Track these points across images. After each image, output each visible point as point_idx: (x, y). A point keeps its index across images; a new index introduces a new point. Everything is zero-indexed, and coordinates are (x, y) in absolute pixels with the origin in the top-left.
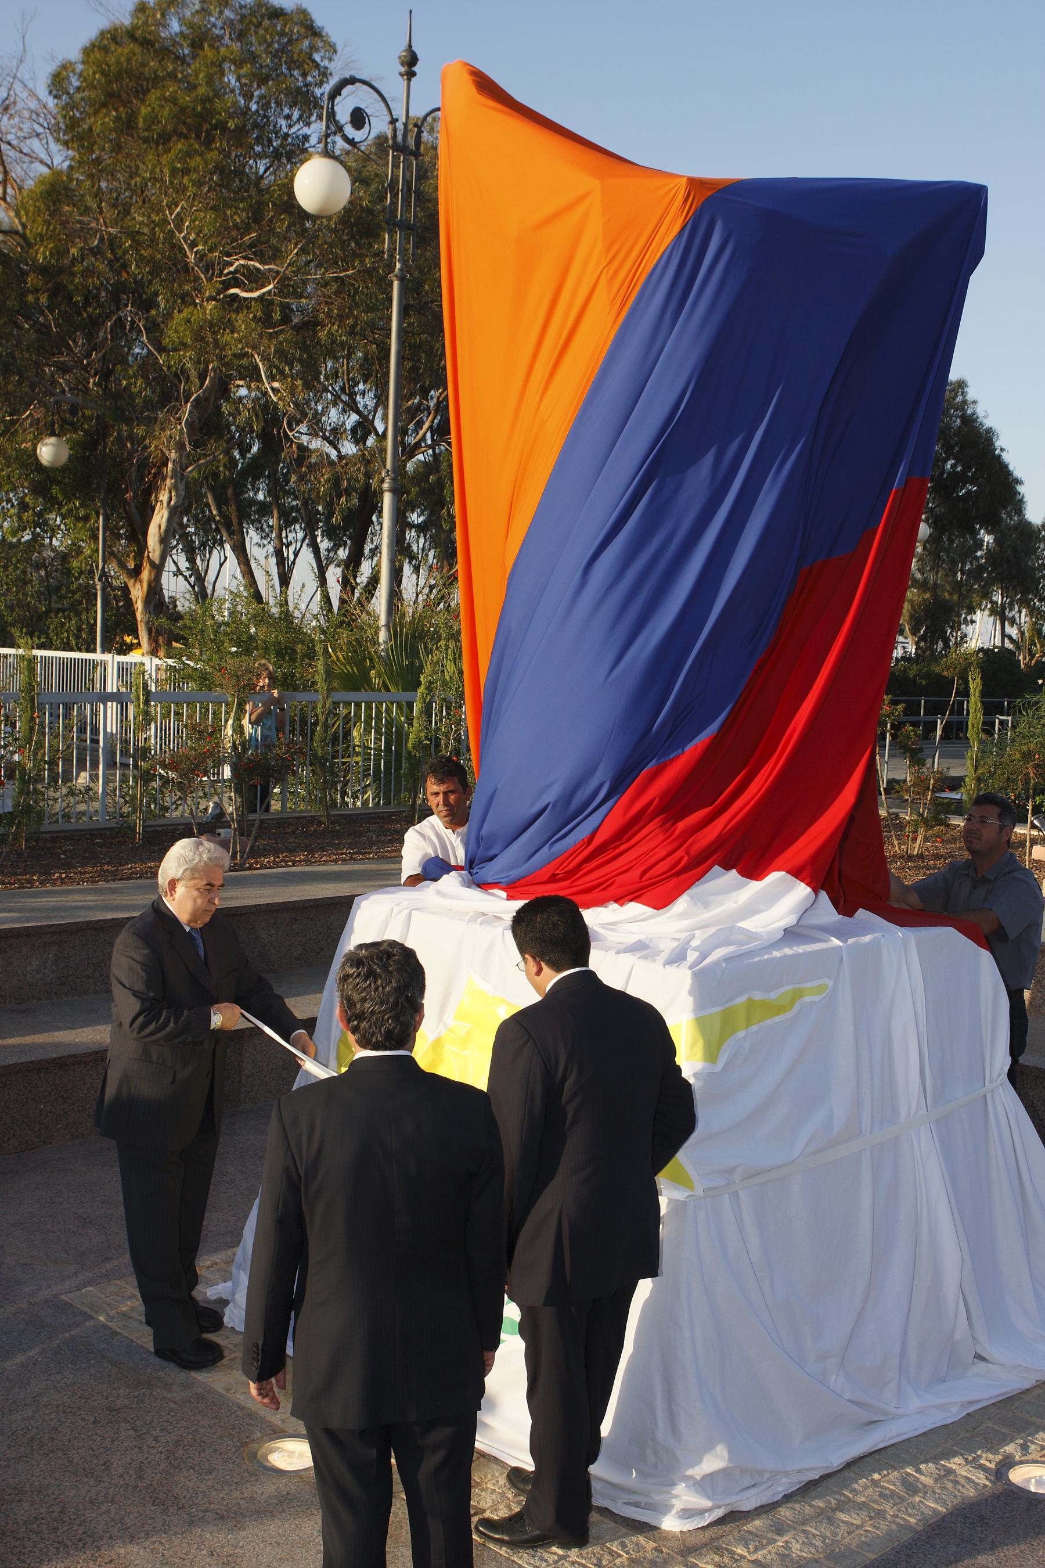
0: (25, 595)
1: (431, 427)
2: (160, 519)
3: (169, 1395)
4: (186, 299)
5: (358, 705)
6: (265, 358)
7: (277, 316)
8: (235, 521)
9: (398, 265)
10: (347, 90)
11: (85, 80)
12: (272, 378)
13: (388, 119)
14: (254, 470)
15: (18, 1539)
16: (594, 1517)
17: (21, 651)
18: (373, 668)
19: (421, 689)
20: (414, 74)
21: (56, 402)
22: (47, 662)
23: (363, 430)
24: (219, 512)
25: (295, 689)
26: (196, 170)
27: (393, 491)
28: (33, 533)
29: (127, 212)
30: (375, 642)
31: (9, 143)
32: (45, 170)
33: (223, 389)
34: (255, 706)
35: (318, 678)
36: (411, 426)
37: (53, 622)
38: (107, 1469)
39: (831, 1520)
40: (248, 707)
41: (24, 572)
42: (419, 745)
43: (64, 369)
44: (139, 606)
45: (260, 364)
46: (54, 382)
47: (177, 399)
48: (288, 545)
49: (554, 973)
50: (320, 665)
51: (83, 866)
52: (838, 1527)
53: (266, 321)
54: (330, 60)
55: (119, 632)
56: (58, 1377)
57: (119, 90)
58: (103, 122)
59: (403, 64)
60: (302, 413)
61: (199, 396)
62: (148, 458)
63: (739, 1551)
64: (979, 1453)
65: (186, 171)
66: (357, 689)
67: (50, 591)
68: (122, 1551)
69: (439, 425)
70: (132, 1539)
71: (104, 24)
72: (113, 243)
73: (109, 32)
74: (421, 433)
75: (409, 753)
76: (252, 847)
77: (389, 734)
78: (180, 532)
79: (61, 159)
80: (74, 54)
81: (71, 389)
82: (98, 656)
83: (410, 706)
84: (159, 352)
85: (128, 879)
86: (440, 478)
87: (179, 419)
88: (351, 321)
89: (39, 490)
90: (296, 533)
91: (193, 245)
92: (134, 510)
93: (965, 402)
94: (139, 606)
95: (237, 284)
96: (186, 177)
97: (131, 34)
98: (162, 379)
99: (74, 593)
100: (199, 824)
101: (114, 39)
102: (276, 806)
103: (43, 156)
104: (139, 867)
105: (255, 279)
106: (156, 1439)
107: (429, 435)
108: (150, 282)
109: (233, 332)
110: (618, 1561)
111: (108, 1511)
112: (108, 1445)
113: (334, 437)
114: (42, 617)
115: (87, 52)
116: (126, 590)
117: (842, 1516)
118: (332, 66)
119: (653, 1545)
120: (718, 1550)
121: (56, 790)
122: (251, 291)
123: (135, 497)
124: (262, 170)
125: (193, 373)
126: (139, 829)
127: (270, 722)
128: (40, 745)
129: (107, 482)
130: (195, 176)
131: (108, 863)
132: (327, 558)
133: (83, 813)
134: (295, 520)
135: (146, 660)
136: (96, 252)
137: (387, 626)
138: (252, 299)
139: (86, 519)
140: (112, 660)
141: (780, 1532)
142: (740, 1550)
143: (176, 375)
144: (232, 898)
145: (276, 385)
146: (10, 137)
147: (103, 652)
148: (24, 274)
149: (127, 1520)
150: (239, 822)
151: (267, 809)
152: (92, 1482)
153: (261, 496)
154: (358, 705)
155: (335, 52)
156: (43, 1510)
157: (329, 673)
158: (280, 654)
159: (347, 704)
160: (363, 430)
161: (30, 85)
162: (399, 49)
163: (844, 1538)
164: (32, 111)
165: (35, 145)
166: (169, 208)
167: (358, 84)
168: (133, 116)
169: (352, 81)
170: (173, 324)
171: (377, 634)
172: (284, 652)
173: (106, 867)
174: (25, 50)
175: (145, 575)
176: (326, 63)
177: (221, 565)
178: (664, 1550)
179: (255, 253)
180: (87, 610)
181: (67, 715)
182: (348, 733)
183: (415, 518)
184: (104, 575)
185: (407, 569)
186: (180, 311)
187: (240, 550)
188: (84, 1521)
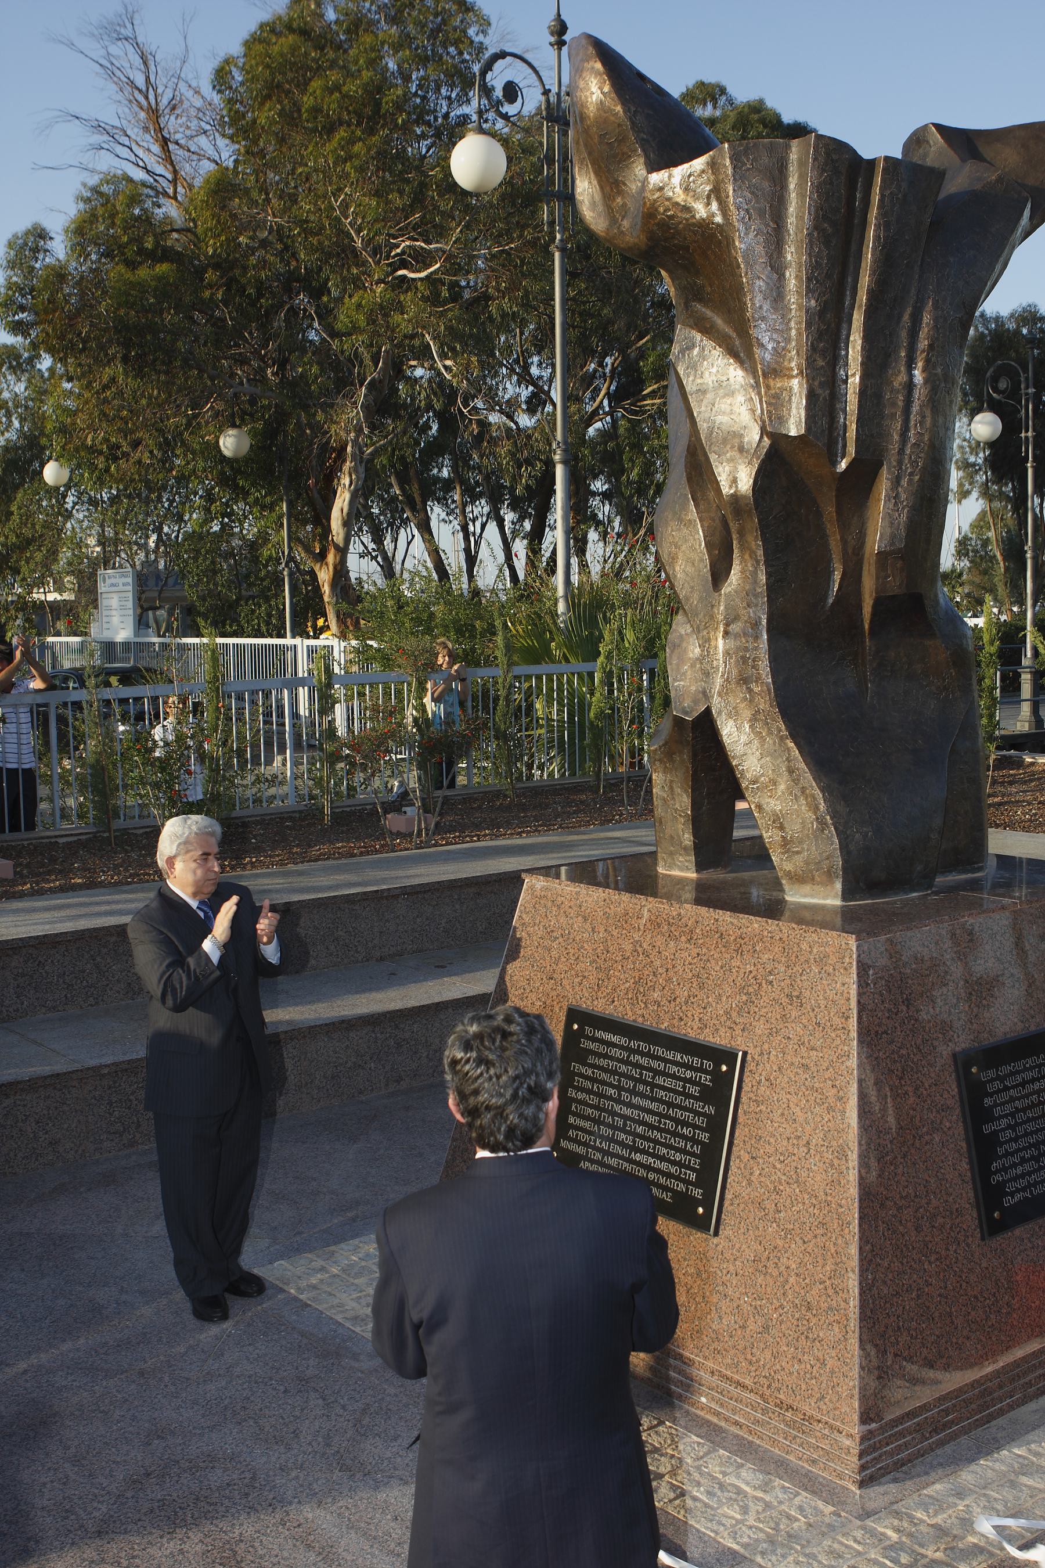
0: (216, 585)
1: (608, 394)
2: (342, 502)
3: (356, 1365)
4: (358, 284)
5: (539, 678)
7: (445, 293)
8: (418, 499)
9: (558, 236)
10: (499, 65)
11: (248, 73)
12: (443, 356)
13: (540, 90)
14: (435, 450)
15: (211, 1504)
17: (205, 640)
18: (553, 640)
19: (601, 659)
21: (235, 395)
22: (239, 649)
23: (537, 402)
24: (403, 490)
25: (477, 664)
26: (357, 156)
27: (564, 462)
28: (222, 523)
29: (294, 199)
30: (554, 615)
31: (177, 143)
32: (212, 166)
33: (397, 369)
34: (435, 684)
35: (498, 653)
36: (588, 394)
37: (243, 610)
38: (297, 1436)
39: (1013, 1484)
40: (429, 686)
41: (213, 562)
42: (601, 715)
43: (242, 361)
44: (326, 589)
46: (233, 375)
47: (352, 384)
48: (474, 521)
50: (499, 639)
51: (273, 849)
52: (1021, 1491)
53: (434, 299)
54: (484, 32)
55: (307, 615)
56: (251, 1349)
57: (282, 80)
58: (267, 115)
60: (477, 388)
61: (373, 379)
62: (328, 442)
63: (919, 1515)
65: (349, 158)
66: (537, 662)
67: (240, 579)
68: (310, 1516)
69: (615, 391)
70: (320, 1503)
71: (265, 16)
72: (280, 232)
73: (267, 24)
74: (598, 400)
75: (591, 723)
76: (437, 824)
77: (571, 705)
78: (364, 514)
79: (227, 155)
80: (236, 49)
81: (248, 380)
82: (288, 641)
83: (591, 675)
84: (332, 338)
85: (316, 860)
86: (618, 444)
87: (355, 403)
89: (224, 481)
90: (482, 507)
91: (358, 232)
92: (316, 495)
94: (326, 589)
95: (404, 265)
97: (290, 28)
98: (336, 366)
99: (262, 580)
100: (383, 803)
101: (273, 31)
102: (461, 780)
103: (211, 152)
104: (325, 848)
105: (422, 259)
106: (344, 1407)
107: (606, 402)
108: (320, 269)
109: (402, 314)
110: (796, 1525)
111: (297, 1477)
112: (298, 1414)
113: (509, 410)
114: (233, 605)
115: (248, 44)
116: (313, 574)
117: (1024, 1480)
118: (487, 41)
119: (831, 1509)
120: (897, 1514)
121: (243, 778)
122: (419, 271)
123: (317, 483)
124: (424, 151)
125: (367, 357)
126: (327, 810)
127: (454, 699)
128: (228, 732)
129: (289, 470)
130: (357, 163)
131: (297, 846)
132: (513, 532)
133: (274, 797)
134: (480, 495)
135: (334, 642)
136: (264, 244)
137: (566, 597)
138: (421, 279)
139: (271, 508)
140: (302, 644)
141: (960, 1495)
142: (920, 1515)
143: (350, 360)
144: (408, 877)
145: (448, 363)
146: (178, 136)
147: (294, 637)
148: (200, 272)
149: (315, 1486)
150: (423, 799)
151: (452, 784)
152: (282, 1449)
153: (445, 473)
154: (539, 678)
155: (489, 24)
156: (235, 1476)
157: (509, 648)
158: (459, 632)
159: (528, 678)
160: (537, 402)
161: (194, 84)
162: (548, 18)
163: (1025, 1501)
164: (199, 109)
165: (203, 141)
166: (334, 195)
167: (508, 58)
168: (297, 107)
169: (503, 55)
170: (344, 309)
171: (556, 604)
172: (462, 630)
173: (295, 850)
174: (187, 50)
175: (331, 558)
176: (480, 38)
177: (409, 544)
178: (843, 1514)
179: (419, 234)
180: (276, 596)
181: (253, 702)
182: (530, 707)
183: (599, 485)
184: (291, 559)
185: (593, 535)
186: (350, 296)
187: (425, 528)
188: (274, 1487)
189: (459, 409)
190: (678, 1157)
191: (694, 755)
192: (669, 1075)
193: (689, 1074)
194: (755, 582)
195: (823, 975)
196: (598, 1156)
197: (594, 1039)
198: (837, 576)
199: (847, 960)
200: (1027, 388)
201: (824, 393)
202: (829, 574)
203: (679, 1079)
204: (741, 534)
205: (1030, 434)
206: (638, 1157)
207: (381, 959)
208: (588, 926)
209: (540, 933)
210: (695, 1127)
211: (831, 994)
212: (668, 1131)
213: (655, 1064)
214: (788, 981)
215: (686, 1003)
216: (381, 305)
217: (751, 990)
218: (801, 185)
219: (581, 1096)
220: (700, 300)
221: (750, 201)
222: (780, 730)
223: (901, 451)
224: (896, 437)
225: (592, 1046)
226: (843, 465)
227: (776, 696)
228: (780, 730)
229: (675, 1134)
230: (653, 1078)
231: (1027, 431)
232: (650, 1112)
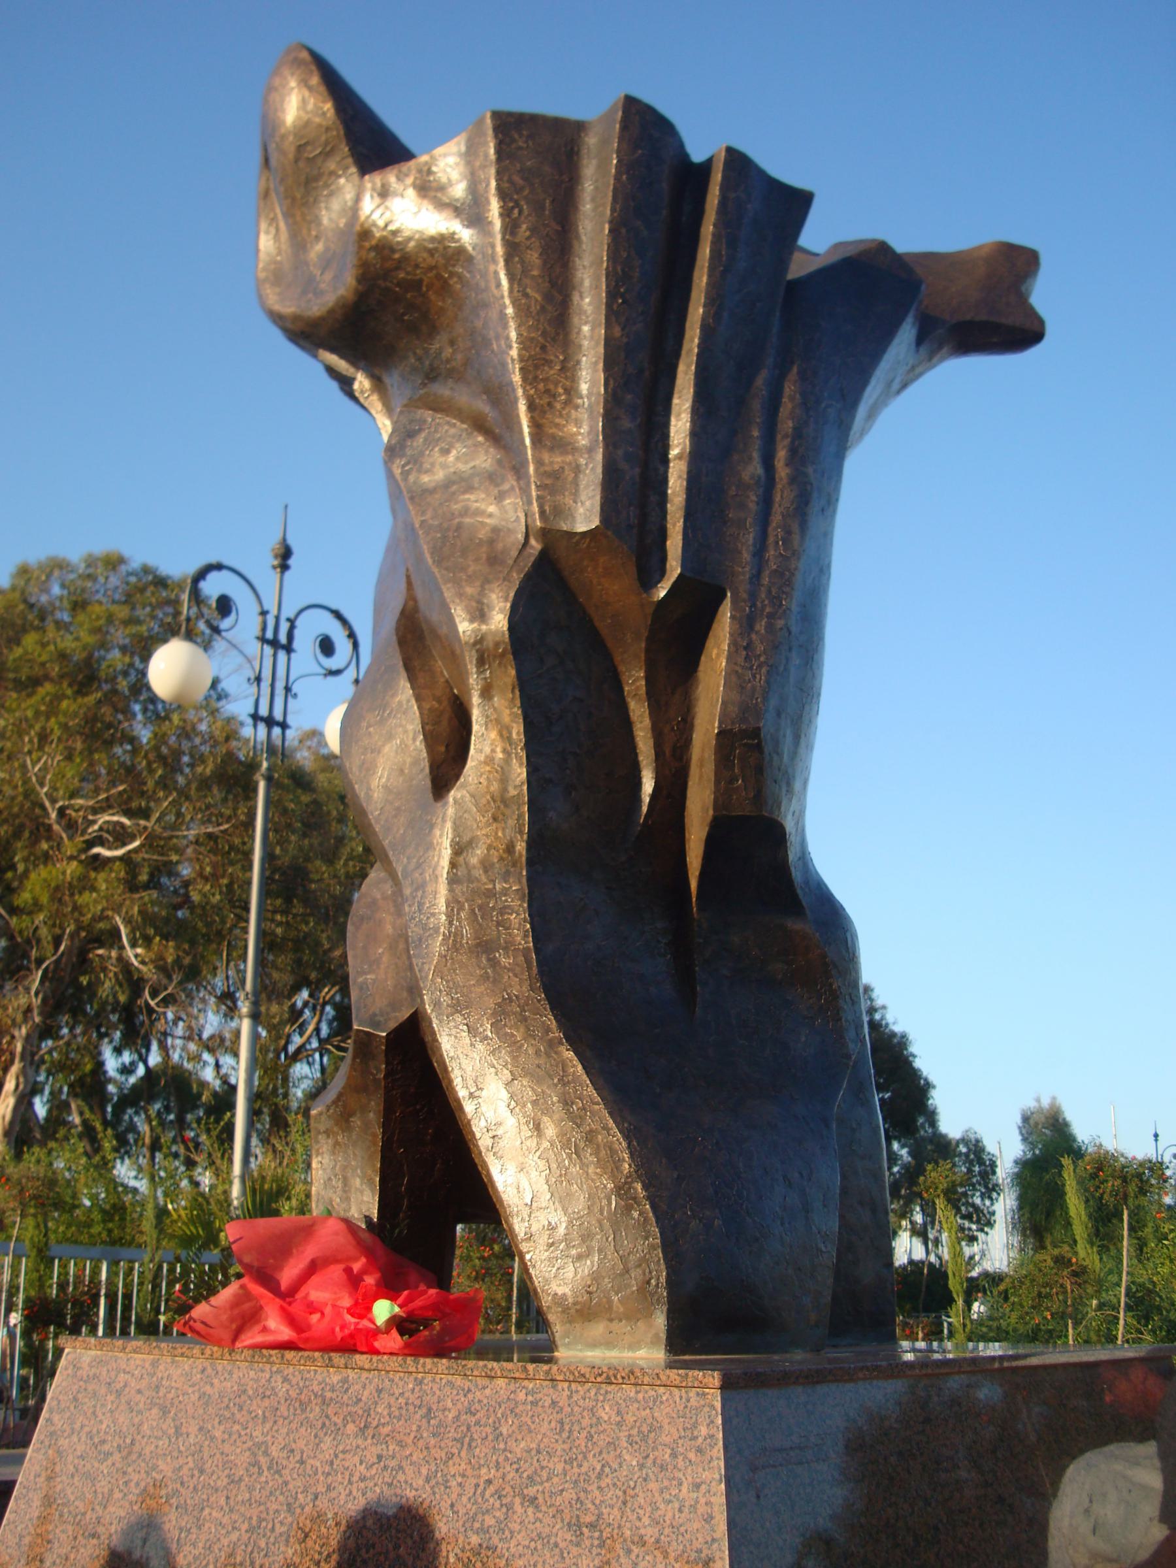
4: (46, 858)
6: (128, 921)
10: (213, 576)
12: (134, 945)
13: (258, 610)
45: (122, 928)
59: (276, 557)
64: (1037, 1152)
69: (324, 987)
88: (225, 881)
95: (99, 841)
96: (53, 720)
105: (120, 836)
122: (116, 848)
162: (272, 541)
167: (225, 573)
169: (219, 567)
189: (146, 1001)
194: (504, 780)
195: (650, 1471)
198: (648, 786)
199: (703, 1430)
201: (632, 473)
202: (638, 784)
204: (486, 693)
208: (168, 1425)
209: (80, 1448)
211: (668, 1512)
214: (570, 1495)
216: (70, 883)
217: (490, 1521)
221: (522, 189)
222: (548, 1030)
223: (757, 576)
224: (746, 556)
227: (541, 972)
228: (548, 1030)
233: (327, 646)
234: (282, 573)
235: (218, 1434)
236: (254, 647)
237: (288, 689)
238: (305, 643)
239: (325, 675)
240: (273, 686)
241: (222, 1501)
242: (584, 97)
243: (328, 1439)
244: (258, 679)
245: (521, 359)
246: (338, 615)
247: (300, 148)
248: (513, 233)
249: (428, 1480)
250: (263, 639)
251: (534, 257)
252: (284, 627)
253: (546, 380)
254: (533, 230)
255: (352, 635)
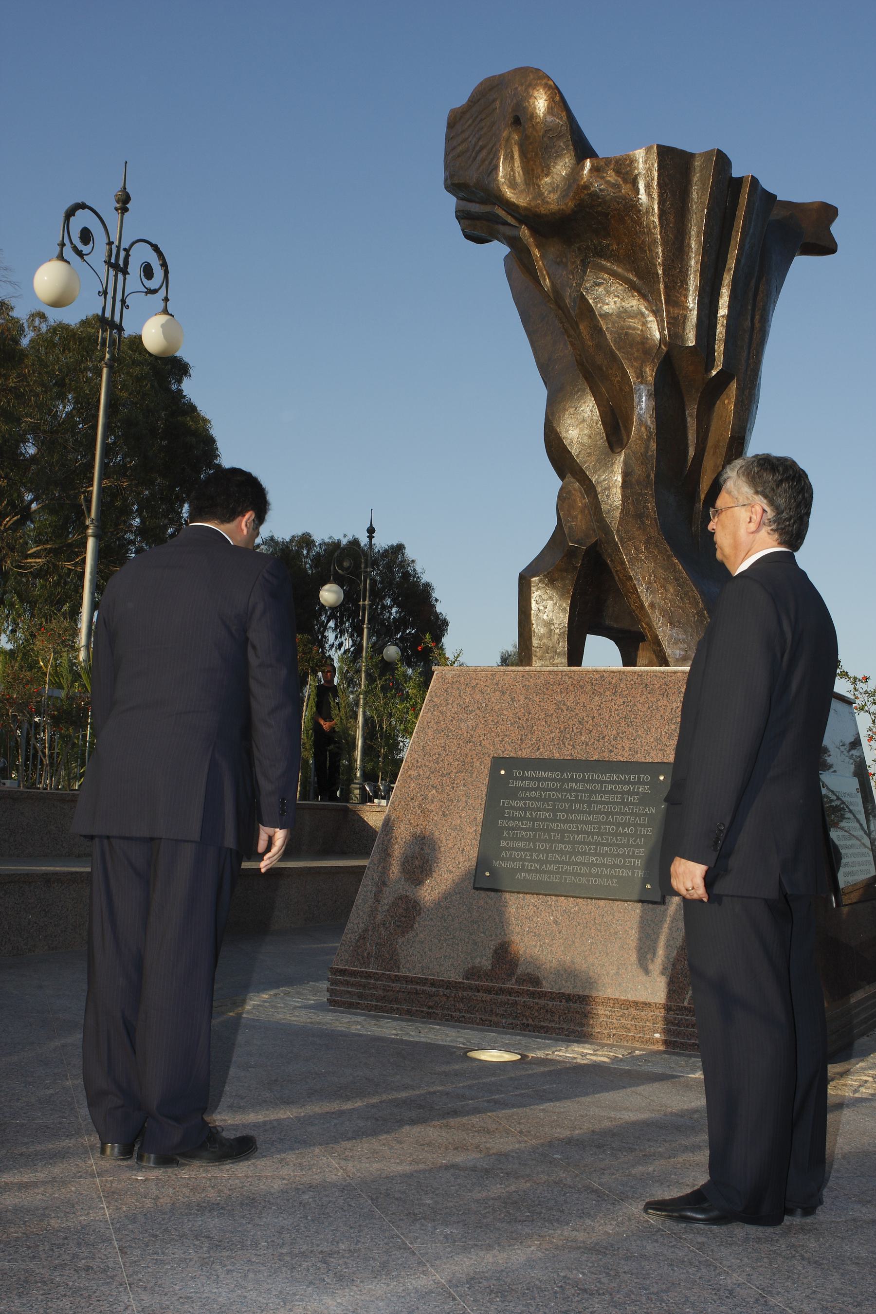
9: (107, 356)
10: (79, 213)
13: (106, 241)
16: (835, 704)
20: (127, 210)
27: (95, 536)
49: (775, 543)
93: (404, 561)
169: (83, 206)
190: (621, 851)
191: (578, 579)
192: (605, 792)
193: (626, 788)
194: (647, 447)
196: (536, 866)
197: (523, 779)
200: (366, 567)
203: (617, 793)
205: (367, 602)
206: (579, 859)
207: (79, 856)
210: (636, 825)
212: (609, 834)
213: (591, 787)
215: (615, 739)
218: (703, 181)
219: (511, 824)
220: (601, 257)
222: (667, 551)
225: (521, 784)
226: (714, 373)
228: (667, 551)
229: (616, 835)
230: (590, 797)
231: (364, 600)
232: (586, 823)
233: (148, 271)
234: (123, 214)
235: (536, 699)
236: (103, 269)
237: (123, 301)
238: (135, 268)
239: (147, 293)
240: (114, 298)
241: (544, 723)
242: (695, 143)
243: (597, 698)
244: (105, 293)
245: (663, 264)
246: (156, 248)
247: (547, 131)
248: (663, 205)
249: (649, 708)
250: (108, 263)
251: (671, 217)
252: (123, 254)
253: (673, 275)
254: (672, 205)
255: (164, 265)
